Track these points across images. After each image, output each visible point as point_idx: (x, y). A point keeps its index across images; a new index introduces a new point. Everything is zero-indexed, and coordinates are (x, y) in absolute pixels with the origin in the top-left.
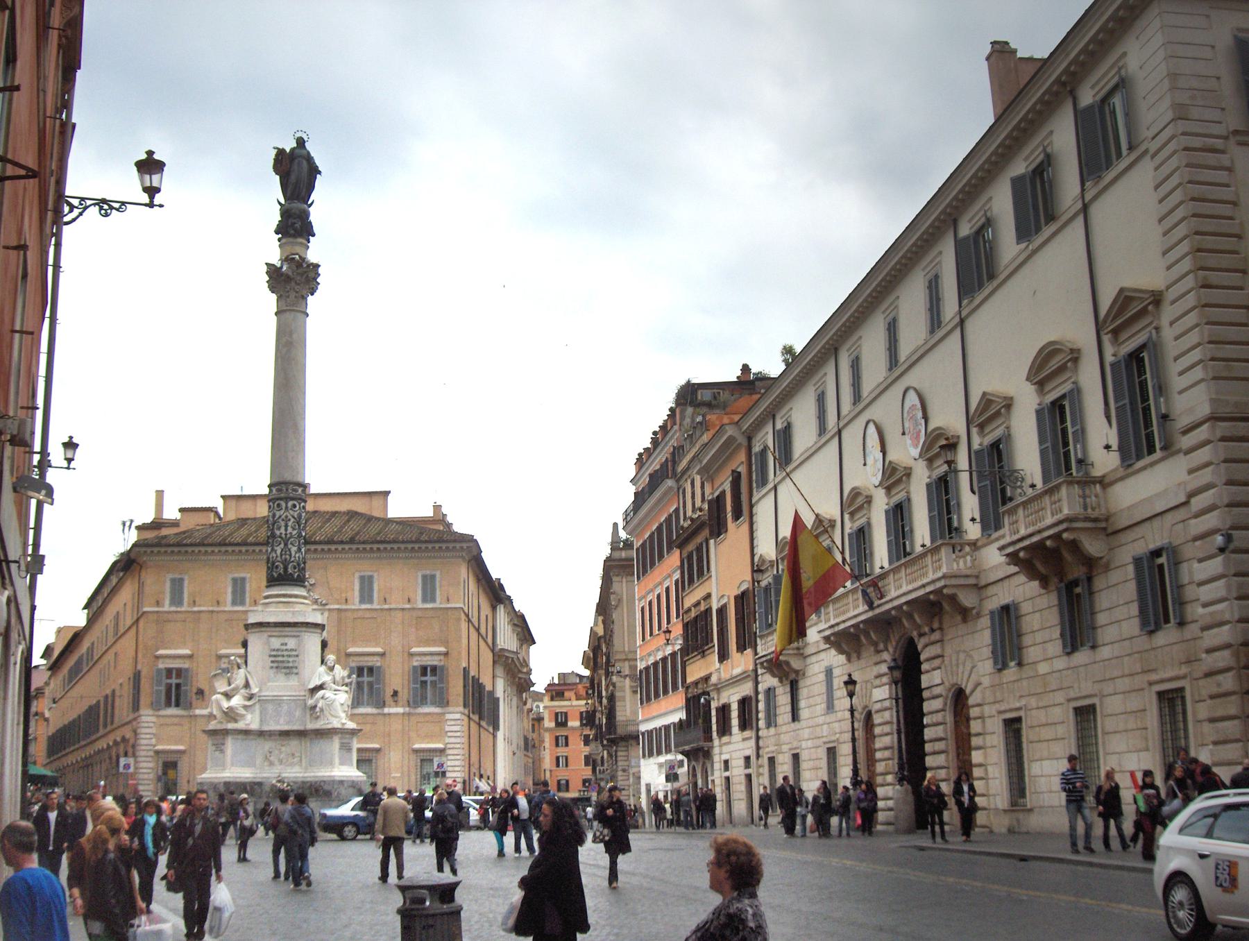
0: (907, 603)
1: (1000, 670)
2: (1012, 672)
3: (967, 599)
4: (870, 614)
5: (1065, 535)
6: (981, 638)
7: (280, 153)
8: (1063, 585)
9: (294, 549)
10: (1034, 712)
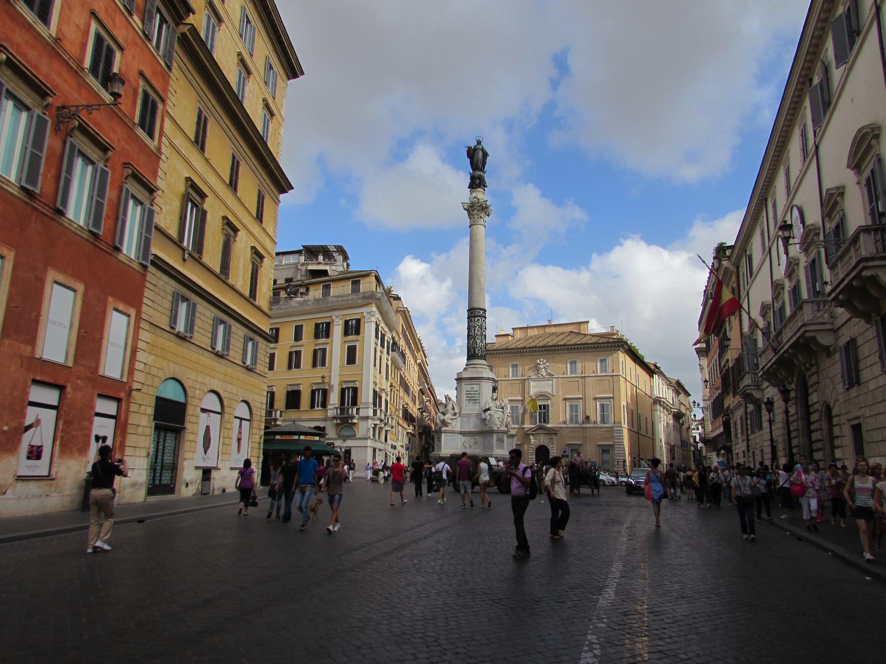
0: (790, 347)
1: (848, 389)
2: (854, 392)
3: (825, 340)
4: (778, 356)
5: (864, 273)
6: (834, 367)
7: (469, 148)
8: (878, 318)
9: (478, 341)
10: (869, 420)
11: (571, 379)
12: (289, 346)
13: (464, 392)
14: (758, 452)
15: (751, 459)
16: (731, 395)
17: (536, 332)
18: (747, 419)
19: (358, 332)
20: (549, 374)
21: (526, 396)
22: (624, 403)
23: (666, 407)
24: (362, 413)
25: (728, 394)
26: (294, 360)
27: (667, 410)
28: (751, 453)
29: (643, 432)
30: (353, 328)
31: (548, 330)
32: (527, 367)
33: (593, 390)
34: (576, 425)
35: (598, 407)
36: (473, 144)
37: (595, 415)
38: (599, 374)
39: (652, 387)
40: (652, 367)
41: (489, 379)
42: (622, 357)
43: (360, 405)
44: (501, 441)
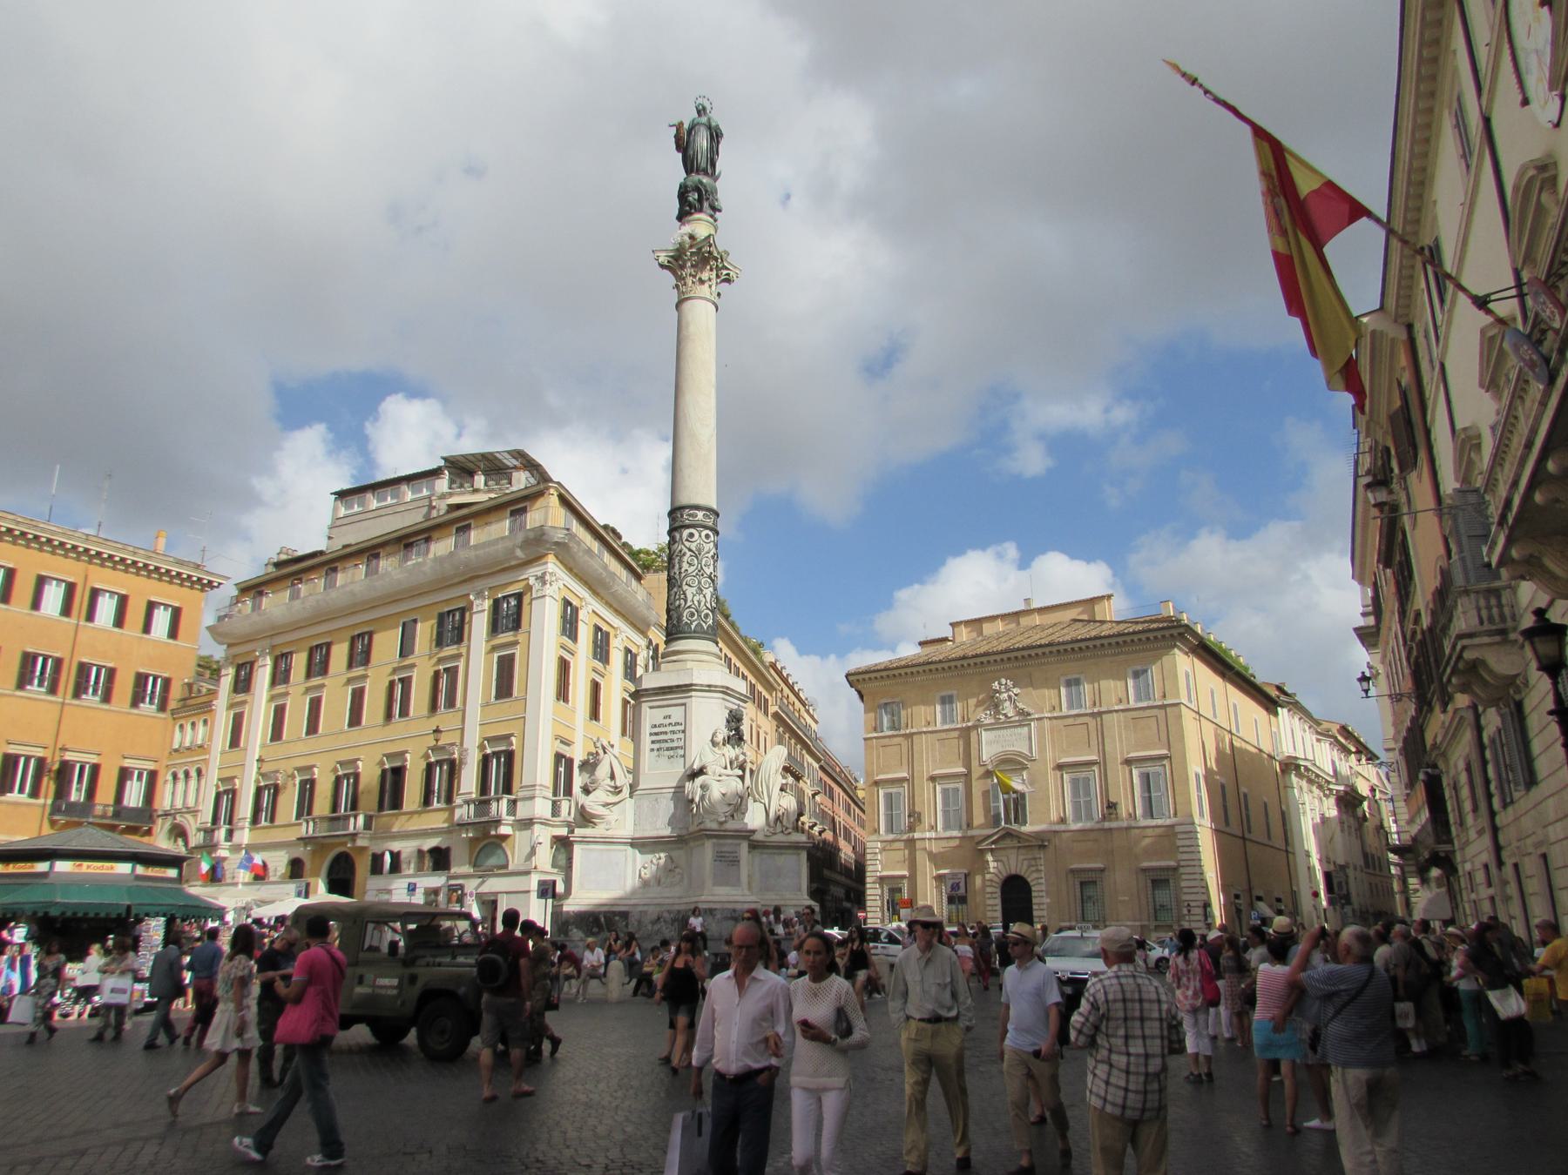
9: (690, 592)
11: (1070, 721)
12: (390, 670)
13: (646, 729)
14: (1531, 866)
15: (1512, 889)
16: (1437, 708)
17: (1000, 626)
18: (1484, 763)
19: (516, 624)
20: (1021, 713)
21: (975, 763)
22: (1195, 768)
23: (1314, 780)
24: (523, 811)
25: (1431, 710)
26: (397, 701)
27: (1320, 787)
28: (1508, 870)
29: (1258, 833)
30: (508, 617)
31: (1024, 621)
32: (972, 702)
33: (1121, 742)
34: (1089, 825)
35: (1136, 780)
36: (689, 116)
37: (1130, 803)
38: (1132, 704)
39: (1275, 738)
40: (1274, 693)
41: (710, 688)
42: (1183, 663)
43: (518, 792)
44: (728, 861)
